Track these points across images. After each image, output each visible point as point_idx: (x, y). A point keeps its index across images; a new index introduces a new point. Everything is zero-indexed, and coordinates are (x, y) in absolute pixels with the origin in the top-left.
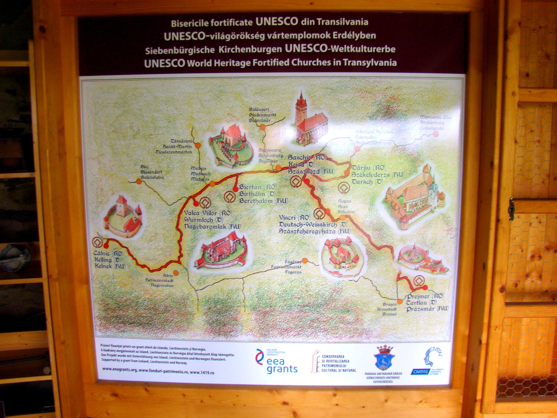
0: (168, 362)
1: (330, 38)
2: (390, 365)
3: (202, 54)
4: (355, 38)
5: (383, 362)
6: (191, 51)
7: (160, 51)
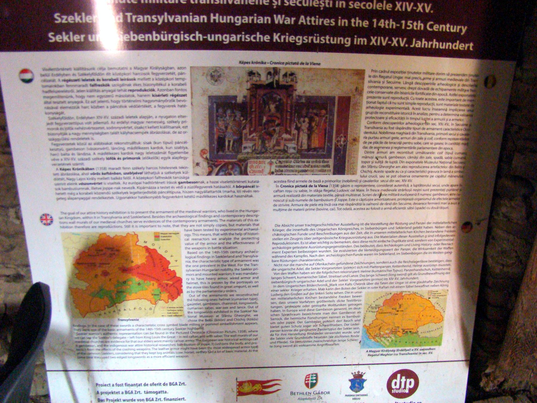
0: (204, 212)
2: (363, 388)
3: (193, 42)
5: (357, 385)
6: (176, 37)
7: (134, 37)
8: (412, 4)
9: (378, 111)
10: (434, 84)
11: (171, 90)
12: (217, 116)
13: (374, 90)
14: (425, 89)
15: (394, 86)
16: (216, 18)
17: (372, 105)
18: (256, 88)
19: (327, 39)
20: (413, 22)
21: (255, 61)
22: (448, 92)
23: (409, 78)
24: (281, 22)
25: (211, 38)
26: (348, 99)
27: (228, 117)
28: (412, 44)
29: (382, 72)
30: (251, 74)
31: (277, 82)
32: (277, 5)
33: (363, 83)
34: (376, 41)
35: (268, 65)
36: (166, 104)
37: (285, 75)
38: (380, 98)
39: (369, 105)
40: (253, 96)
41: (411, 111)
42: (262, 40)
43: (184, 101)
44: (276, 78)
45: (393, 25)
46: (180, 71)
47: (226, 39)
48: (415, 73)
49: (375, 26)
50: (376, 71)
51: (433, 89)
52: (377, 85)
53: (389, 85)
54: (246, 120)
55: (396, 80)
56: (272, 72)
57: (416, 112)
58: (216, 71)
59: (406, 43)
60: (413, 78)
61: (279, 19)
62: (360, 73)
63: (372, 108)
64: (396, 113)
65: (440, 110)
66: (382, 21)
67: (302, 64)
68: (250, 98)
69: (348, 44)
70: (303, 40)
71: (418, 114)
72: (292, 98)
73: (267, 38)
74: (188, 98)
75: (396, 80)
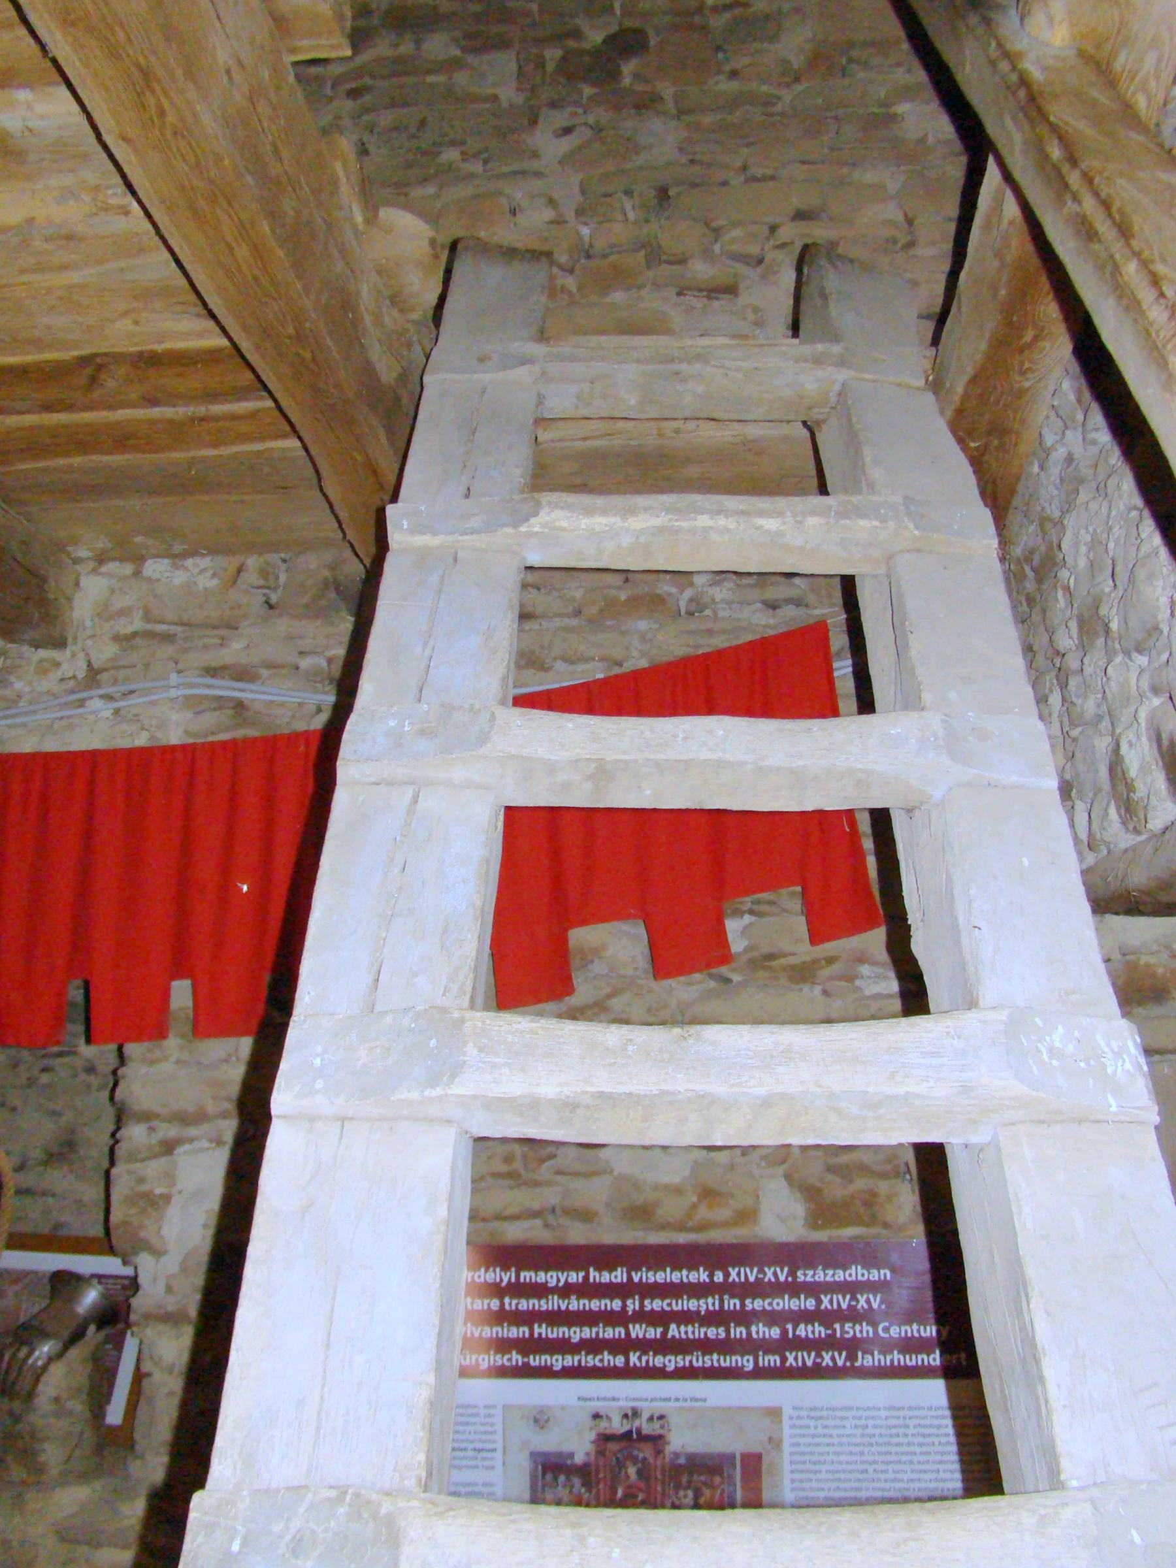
1: (707, 1280)
4: (501, 1280)
8: (813, 1354)
9: (811, 1476)
10: (907, 1427)
11: (472, 1441)
12: (544, 1486)
13: (801, 1440)
14: (891, 1436)
15: (835, 1432)
16: (542, 1330)
17: (800, 1467)
18: (605, 1438)
19: (714, 1360)
20: (854, 1326)
21: (602, 1395)
22: (936, 1440)
23: (860, 1418)
24: (641, 1336)
25: (535, 1361)
26: (758, 1457)
27: (560, 1488)
28: (857, 1360)
29: (811, 1409)
30: (597, 1416)
31: (639, 1431)
32: (634, 1310)
33: (781, 1429)
34: (796, 1358)
35: (621, 1403)
36: (464, 1463)
37: (651, 1419)
38: (812, 1453)
39: (794, 1467)
40: (601, 1453)
41: (871, 1475)
42: (612, 1364)
43: (493, 1459)
44: (637, 1423)
45: (820, 1332)
46: (487, 1411)
47: (558, 1362)
48: (869, 1409)
49: (790, 1335)
50: (801, 1409)
51: (906, 1435)
52: (803, 1431)
53: (826, 1431)
54: (590, 1492)
55: (838, 1422)
56: (630, 1414)
57: (883, 1476)
58: (542, 1412)
59: (846, 1359)
60: (867, 1418)
61: (637, 1331)
62: (774, 1413)
63: (801, 1471)
64: (845, 1480)
65: (925, 1472)
66: (802, 1326)
67: (677, 1400)
68: (596, 1457)
69: (750, 1366)
70: (676, 1362)
71: (886, 1481)
72: (664, 1458)
73: (619, 1361)
74: (499, 1454)
75: (838, 1422)
